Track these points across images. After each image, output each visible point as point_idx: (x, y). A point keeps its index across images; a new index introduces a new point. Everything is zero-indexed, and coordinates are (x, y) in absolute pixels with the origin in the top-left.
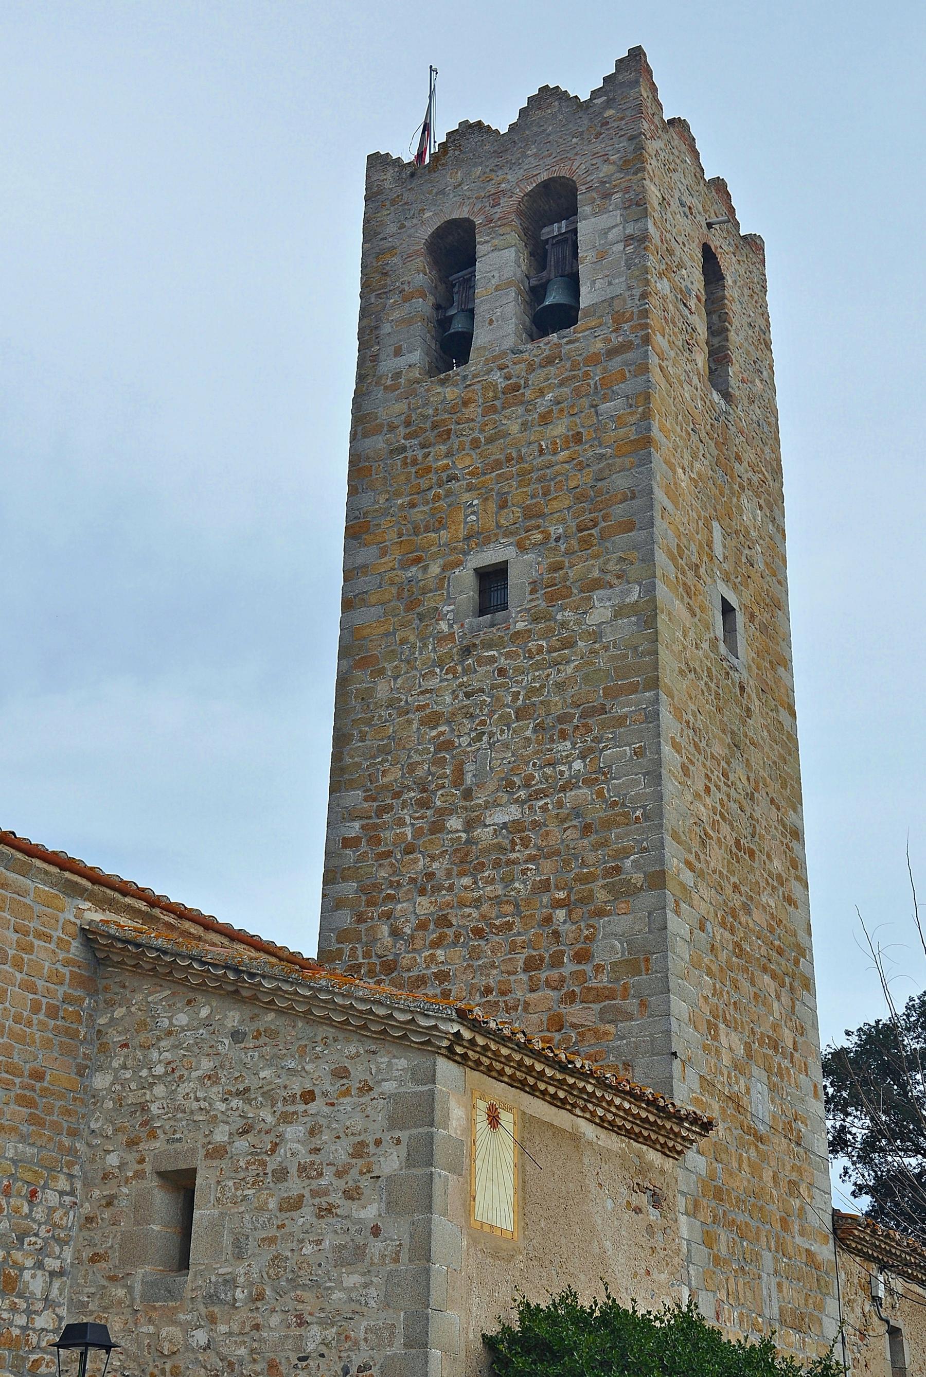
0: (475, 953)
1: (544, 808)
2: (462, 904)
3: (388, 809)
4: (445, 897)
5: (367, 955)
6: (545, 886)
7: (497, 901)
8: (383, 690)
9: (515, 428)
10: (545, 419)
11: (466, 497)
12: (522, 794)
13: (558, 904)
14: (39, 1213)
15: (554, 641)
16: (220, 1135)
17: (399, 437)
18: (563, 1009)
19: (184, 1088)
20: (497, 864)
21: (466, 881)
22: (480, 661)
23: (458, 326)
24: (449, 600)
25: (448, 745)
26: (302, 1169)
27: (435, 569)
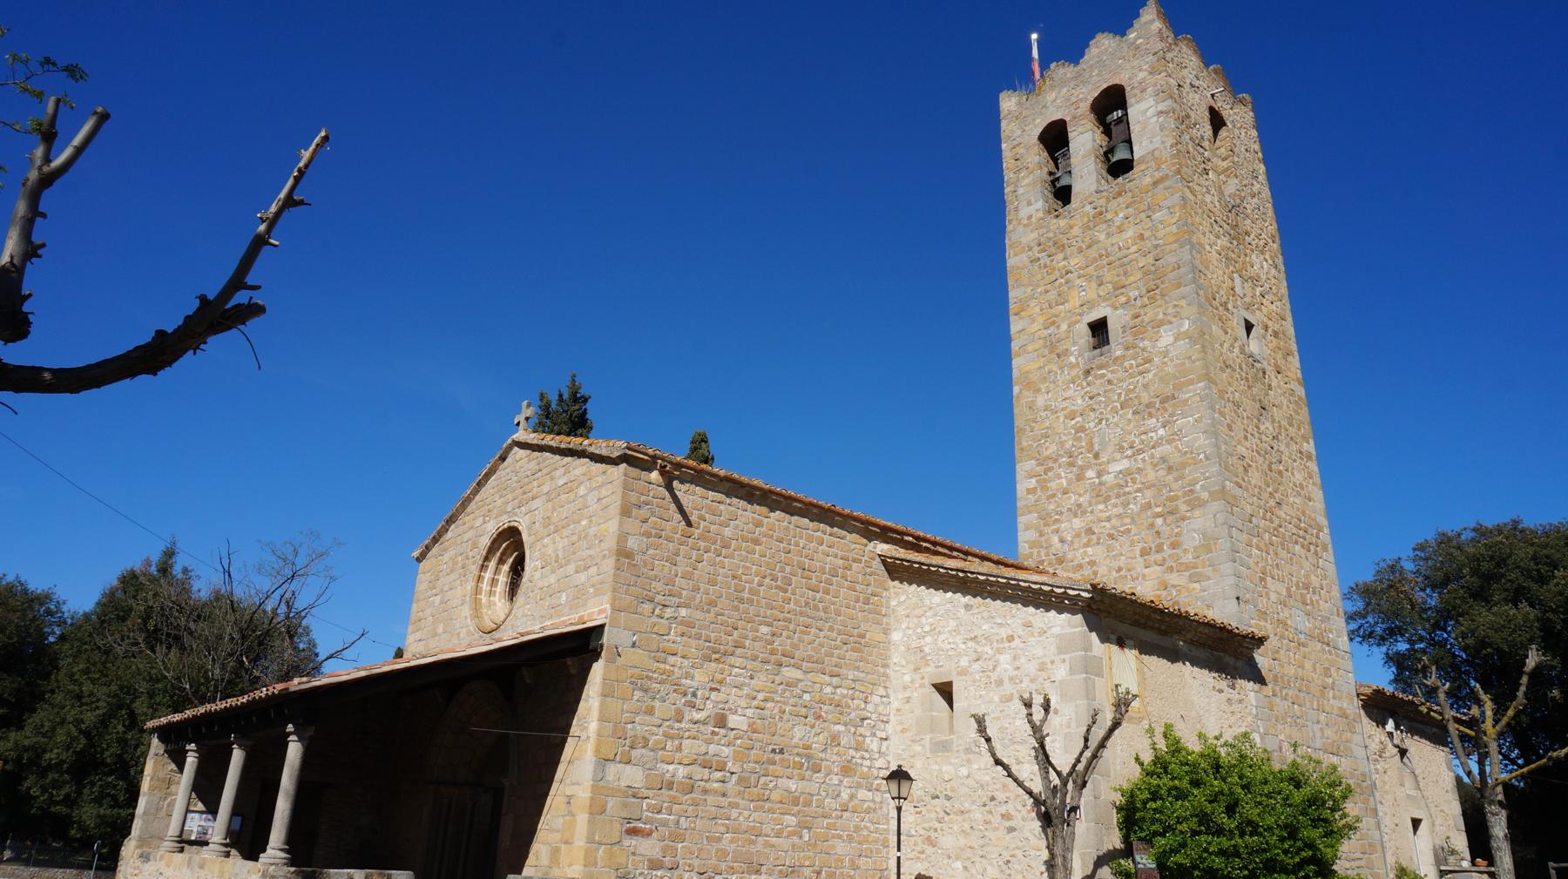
0: (1109, 549)
1: (1143, 460)
2: (1100, 521)
3: (1050, 469)
4: (1090, 517)
5: (1047, 555)
6: (1148, 506)
7: (1119, 516)
8: (1041, 401)
9: (1102, 237)
10: (1121, 230)
11: (1078, 282)
12: (1129, 452)
13: (1159, 515)
14: (870, 707)
15: (1140, 360)
16: (964, 662)
17: (1035, 253)
18: (1166, 577)
19: (942, 637)
20: (1118, 496)
21: (1101, 507)
22: (1096, 377)
23: (1063, 182)
24: (1074, 343)
25: (1081, 429)
26: (1011, 679)
27: (1064, 327)
